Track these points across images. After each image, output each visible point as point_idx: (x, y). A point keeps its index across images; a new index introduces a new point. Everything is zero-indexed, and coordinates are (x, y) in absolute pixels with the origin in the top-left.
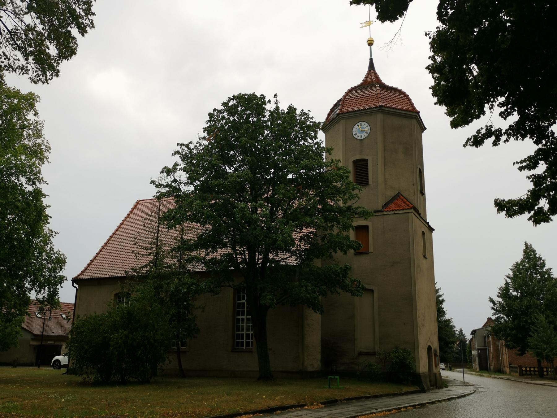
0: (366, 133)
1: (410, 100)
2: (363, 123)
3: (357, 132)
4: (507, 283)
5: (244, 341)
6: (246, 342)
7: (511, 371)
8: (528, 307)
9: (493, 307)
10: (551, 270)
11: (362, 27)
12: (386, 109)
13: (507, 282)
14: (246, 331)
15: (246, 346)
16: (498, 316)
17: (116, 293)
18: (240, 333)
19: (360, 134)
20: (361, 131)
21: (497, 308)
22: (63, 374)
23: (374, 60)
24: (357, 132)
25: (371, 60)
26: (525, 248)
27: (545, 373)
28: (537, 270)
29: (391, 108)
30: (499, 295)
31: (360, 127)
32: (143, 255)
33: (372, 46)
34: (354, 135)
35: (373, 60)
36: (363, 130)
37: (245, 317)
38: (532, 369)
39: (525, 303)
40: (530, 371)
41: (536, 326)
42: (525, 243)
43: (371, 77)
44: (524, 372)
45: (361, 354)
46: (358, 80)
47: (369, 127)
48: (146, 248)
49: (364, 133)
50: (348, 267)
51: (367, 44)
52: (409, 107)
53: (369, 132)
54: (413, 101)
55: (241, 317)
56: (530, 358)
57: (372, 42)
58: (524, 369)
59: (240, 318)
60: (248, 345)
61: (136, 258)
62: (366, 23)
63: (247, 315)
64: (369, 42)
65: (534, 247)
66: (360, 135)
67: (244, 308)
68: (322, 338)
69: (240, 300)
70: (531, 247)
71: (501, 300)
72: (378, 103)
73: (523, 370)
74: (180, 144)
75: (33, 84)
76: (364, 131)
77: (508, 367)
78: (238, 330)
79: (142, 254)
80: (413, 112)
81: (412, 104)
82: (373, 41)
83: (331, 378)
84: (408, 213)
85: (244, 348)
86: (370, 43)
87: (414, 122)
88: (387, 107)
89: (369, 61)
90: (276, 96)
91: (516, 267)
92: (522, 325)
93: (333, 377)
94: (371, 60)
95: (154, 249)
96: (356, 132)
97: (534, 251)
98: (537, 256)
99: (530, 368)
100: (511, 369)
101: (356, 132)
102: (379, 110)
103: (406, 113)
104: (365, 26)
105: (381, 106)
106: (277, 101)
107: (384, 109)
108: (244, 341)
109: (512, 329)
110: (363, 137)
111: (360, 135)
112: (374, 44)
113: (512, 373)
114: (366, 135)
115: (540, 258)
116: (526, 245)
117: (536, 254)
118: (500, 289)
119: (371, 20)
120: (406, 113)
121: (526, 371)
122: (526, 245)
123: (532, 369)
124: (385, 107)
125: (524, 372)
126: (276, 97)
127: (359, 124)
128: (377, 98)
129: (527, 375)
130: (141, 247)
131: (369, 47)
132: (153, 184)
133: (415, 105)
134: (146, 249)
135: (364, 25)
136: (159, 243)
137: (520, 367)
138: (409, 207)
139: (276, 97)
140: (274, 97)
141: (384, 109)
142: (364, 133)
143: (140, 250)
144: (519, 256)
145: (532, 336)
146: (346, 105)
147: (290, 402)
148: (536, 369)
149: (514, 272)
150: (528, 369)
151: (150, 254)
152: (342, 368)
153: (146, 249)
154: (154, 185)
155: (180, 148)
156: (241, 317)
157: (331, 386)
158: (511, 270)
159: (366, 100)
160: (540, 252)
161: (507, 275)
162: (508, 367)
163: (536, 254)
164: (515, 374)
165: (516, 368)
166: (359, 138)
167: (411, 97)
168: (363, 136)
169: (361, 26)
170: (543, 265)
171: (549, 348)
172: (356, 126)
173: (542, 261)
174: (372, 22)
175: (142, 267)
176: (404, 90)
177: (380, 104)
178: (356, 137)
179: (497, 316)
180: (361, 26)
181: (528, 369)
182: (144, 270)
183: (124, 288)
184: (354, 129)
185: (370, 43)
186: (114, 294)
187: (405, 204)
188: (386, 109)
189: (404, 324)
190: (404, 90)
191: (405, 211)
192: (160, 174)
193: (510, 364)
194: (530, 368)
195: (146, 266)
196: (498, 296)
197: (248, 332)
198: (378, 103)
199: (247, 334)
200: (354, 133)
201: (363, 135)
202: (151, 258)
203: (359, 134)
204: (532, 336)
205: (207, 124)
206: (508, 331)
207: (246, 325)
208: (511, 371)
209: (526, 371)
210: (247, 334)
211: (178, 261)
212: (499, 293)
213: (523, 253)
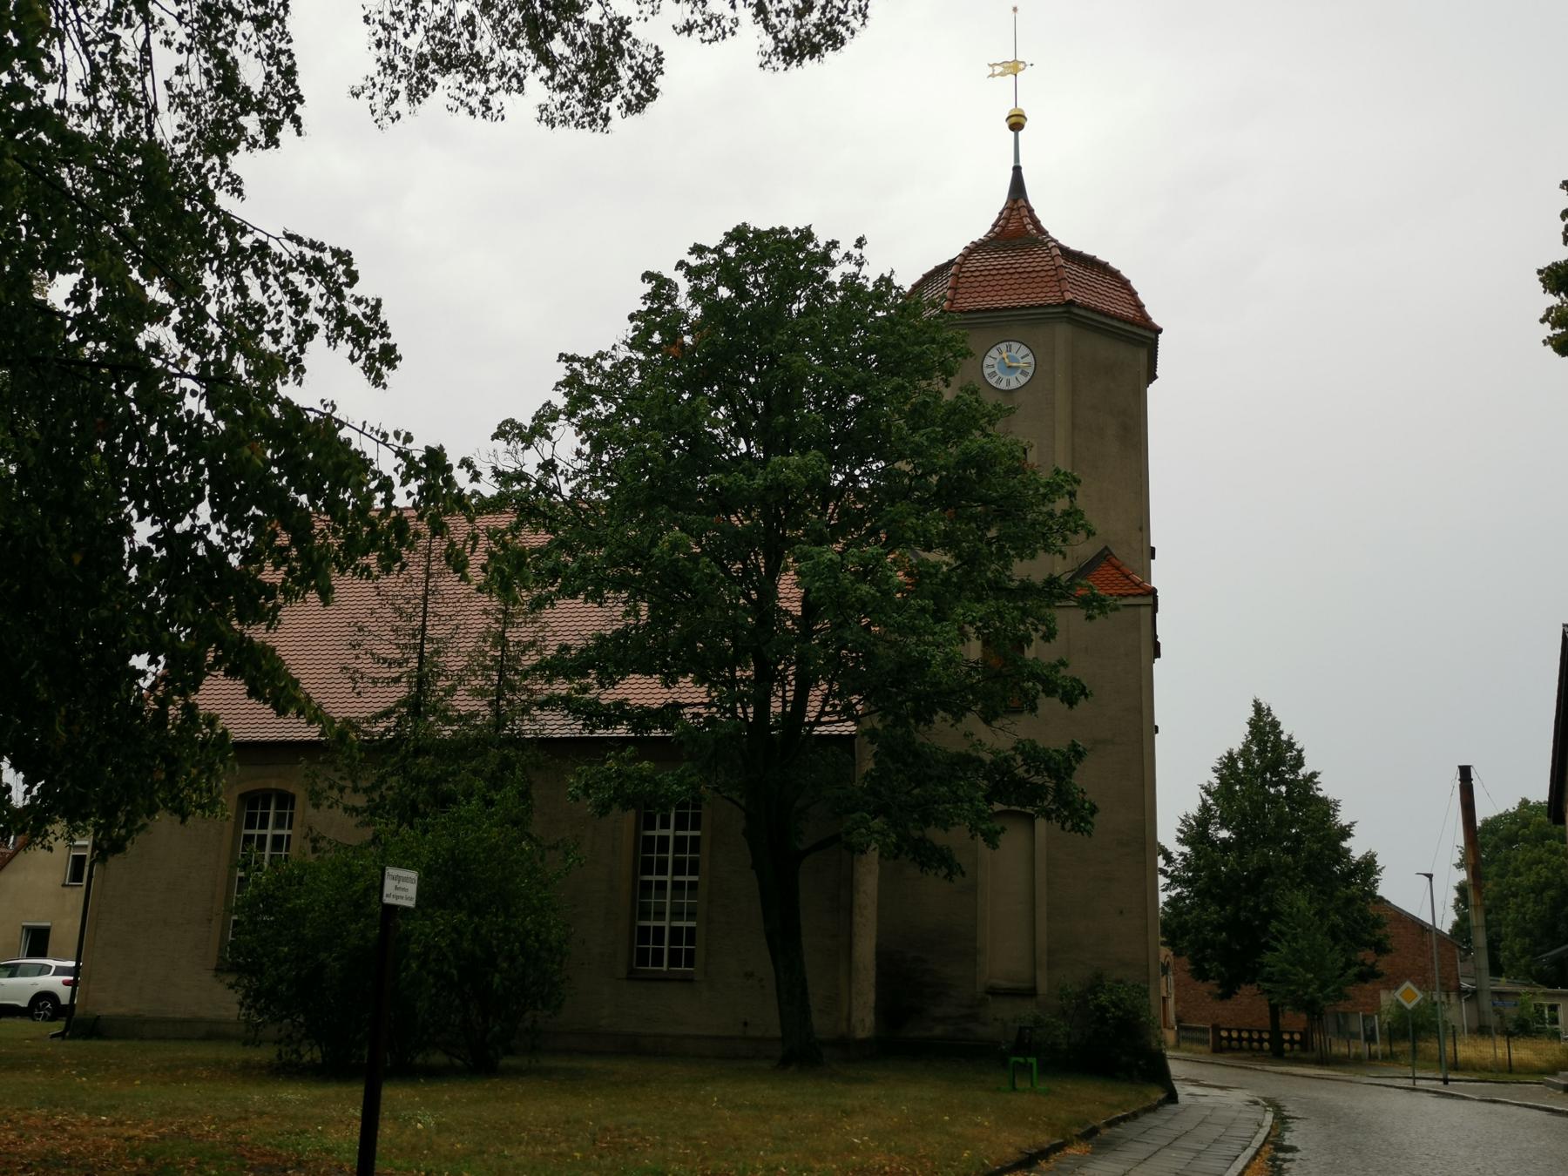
0: (1024, 373)
1: (1133, 294)
2: (1015, 346)
3: (996, 369)
4: (1205, 808)
5: (666, 947)
6: (671, 951)
7: (1183, 1038)
8: (1264, 871)
9: (1166, 868)
10: (1316, 777)
11: (993, 75)
12: (1082, 312)
13: (1204, 802)
14: (671, 920)
15: (670, 964)
16: (1178, 894)
17: (242, 792)
18: (652, 923)
19: (1010, 374)
20: (1009, 367)
21: (1173, 871)
22: (53, 1036)
23: (1024, 172)
24: (996, 369)
25: (1017, 170)
26: (1252, 714)
27: (1287, 1046)
28: (1281, 775)
29: (1094, 310)
30: (1182, 836)
31: (1004, 355)
32: (375, 681)
33: (1020, 133)
34: (986, 376)
35: (1023, 171)
36: (1014, 364)
37: (668, 878)
38: (1245, 1035)
39: (1255, 860)
40: (1240, 1039)
41: (1281, 921)
42: (1255, 701)
43: (1021, 218)
44: (1225, 1043)
45: (994, 992)
46: (980, 226)
47: (1030, 359)
48: (385, 660)
49: (1018, 374)
50: (1081, 749)
51: (1006, 126)
52: (1129, 312)
53: (1030, 371)
54: (1142, 297)
55: (654, 878)
56: (1250, 1004)
57: (1022, 119)
58: (1224, 1034)
59: (651, 881)
60: (675, 959)
61: (354, 688)
62: (1005, 65)
63: (675, 873)
64: (1013, 120)
65: (1278, 714)
66: (1005, 378)
67: (667, 852)
68: (878, 946)
69: (654, 829)
70: (1269, 714)
71: (1186, 849)
72: (1059, 294)
73: (1222, 1038)
74: (565, 356)
75: (650, 107)
76: (1017, 368)
77: (1173, 1028)
78: (645, 914)
79: (373, 678)
80: (1138, 326)
81: (1140, 307)
82: (1023, 116)
83: (1017, 1062)
84: (1139, 605)
85: (665, 968)
86: (1016, 122)
87: (1143, 355)
88: (1087, 308)
89: (1010, 173)
90: (860, 243)
91: (1225, 766)
92: (1242, 918)
93: (1021, 1060)
94: (1017, 170)
95: (414, 663)
96: (992, 370)
97: (1275, 725)
98: (1284, 737)
99: (1260, 1032)
100: (1183, 1033)
101: (992, 370)
102: (1065, 312)
103: (1128, 327)
104: (1002, 74)
105: (1071, 303)
106: (862, 257)
107: (1076, 311)
108: (666, 947)
109: (1218, 928)
110: (1014, 385)
111: (1005, 378)
112: (1027, 125)
113: (1183, 1045)
114: (1023, 380)
115: (1290, 745)
116: (1258, 707)
117: (1282, 732)
118: (1183, 821)
119: (1019, 59)
120: (1128, 327)
121: (1230, 1038)
122: (1258, 707)
123: (1235, 1035)
124: (1080, 306)
125: (1225, 1043)
126: (861, 247)
127: (1003, 346)
128: (1055, 279)
129: (1231, 1049)
130: (372, 654)
131: (1013, 133)
132: (465, 469)
133: (1149, 310)
134: (391, 663)
135: (998, 69)
136: (428, 647)
137: (1216, 1029)
138: (1140, 591)
139: (861, 247)
140: (856, 246)
141: (1076, 311)
142: (1018, 374)
143: (366, 665)
144: (1236, 736)
145: (1276, 950)
146: (964, 290)
147: (1044, 1139)
148: (1266, 1036)
149: (1221, 778)
150: (1255, 1036)
151: (397, 680)
152: (938, 1030)
153: (391, 663)
154: (468, 472)
155: (567, 368)
156: (654, 878)
157: (1018, 1087)
158: (1215, 771)
159: (987, 283)
160: (1289, 728)
161: (1206, 784)
162: (1173, 1028)
163: (1282, 732)
164: (1201, 1048)
165: (1205, 1031)
166: (1003, 386)
167: (1135, 285)
168: (1016, 381)
169: (990, 71)
170: (1299, 761)
171: (1317, 982)
172: (994, 352)
173: (1295, 753)
174: (1022, 66)
175: (378, 717)
176: (1114, 264)
177: (1069, 296)
178: (992, 381)
179: (1173, 893)
180: (990, 71)
181: (1235, 1035)
182: (380, 727)
183: (317, 776)
184: (988, 361)
185: (1016, 122)
186: (236, 794)
187: (1127, 581)
188: (1082, 312)
189: (1121, 912)
190: (1114, 264)
191: (1131, 601)
192: (493, 439)
193: (1179, 1020)
194: (1240, 1031)
195: (387, 714)
196: (1179, 840)
197: (677, 924)
198: (1059, 294)
199: (673, 929)
200: (987, 371)
201: (1012, 378)
202: (401, 691)
203: (1002, 376)
204: (1276, 950)
205: (645, 303)
206: (1208, 933)
207: (672, 903)
208: (1183, 1038)
209: (1230, 1038)
210: (673, 929)
211: (490, 704)
212: (1180, 831)
213: (1247, 729)
